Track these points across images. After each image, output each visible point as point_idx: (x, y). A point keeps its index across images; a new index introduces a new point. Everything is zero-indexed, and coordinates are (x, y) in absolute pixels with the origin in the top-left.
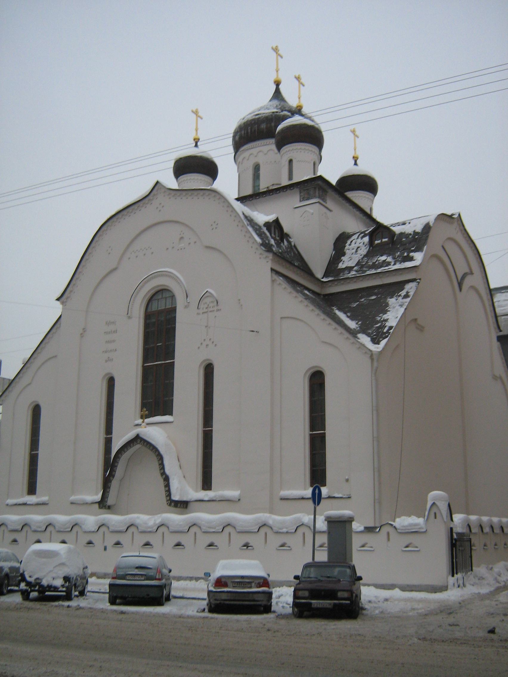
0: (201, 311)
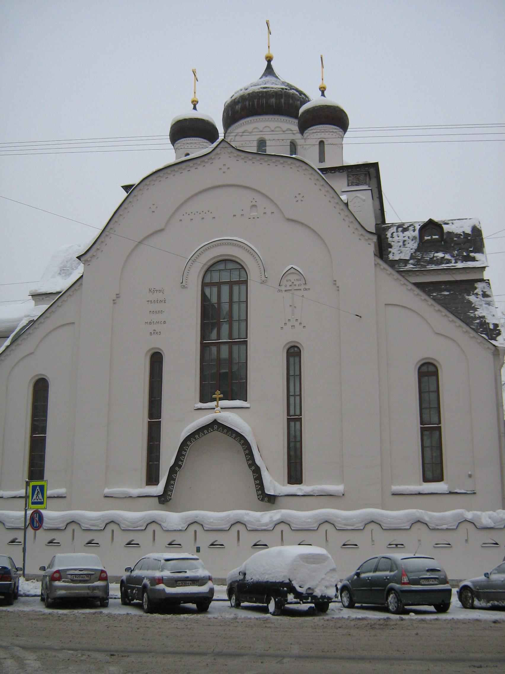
0: (283, 288)
